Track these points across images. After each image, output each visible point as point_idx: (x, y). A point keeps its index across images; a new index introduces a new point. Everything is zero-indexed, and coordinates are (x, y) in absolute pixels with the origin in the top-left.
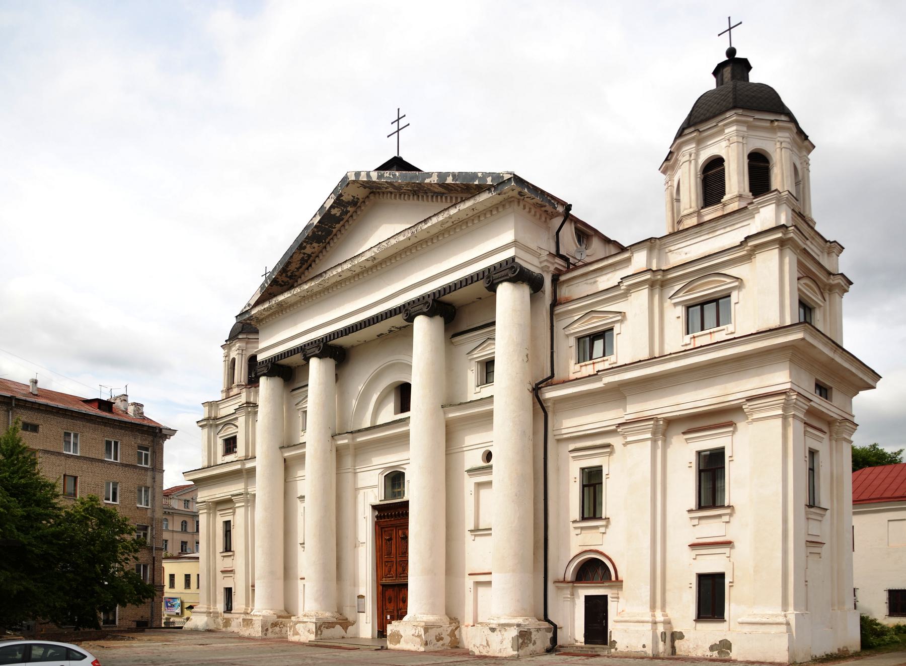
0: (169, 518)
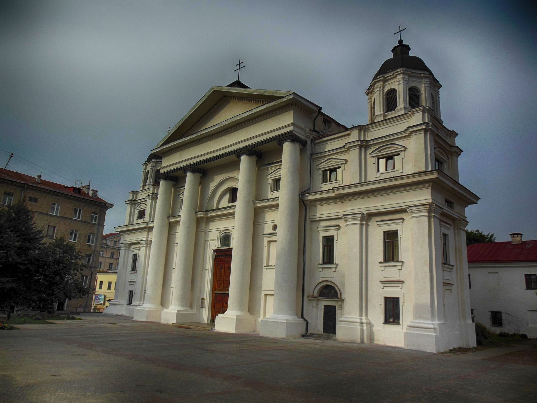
0: (104, 250)
